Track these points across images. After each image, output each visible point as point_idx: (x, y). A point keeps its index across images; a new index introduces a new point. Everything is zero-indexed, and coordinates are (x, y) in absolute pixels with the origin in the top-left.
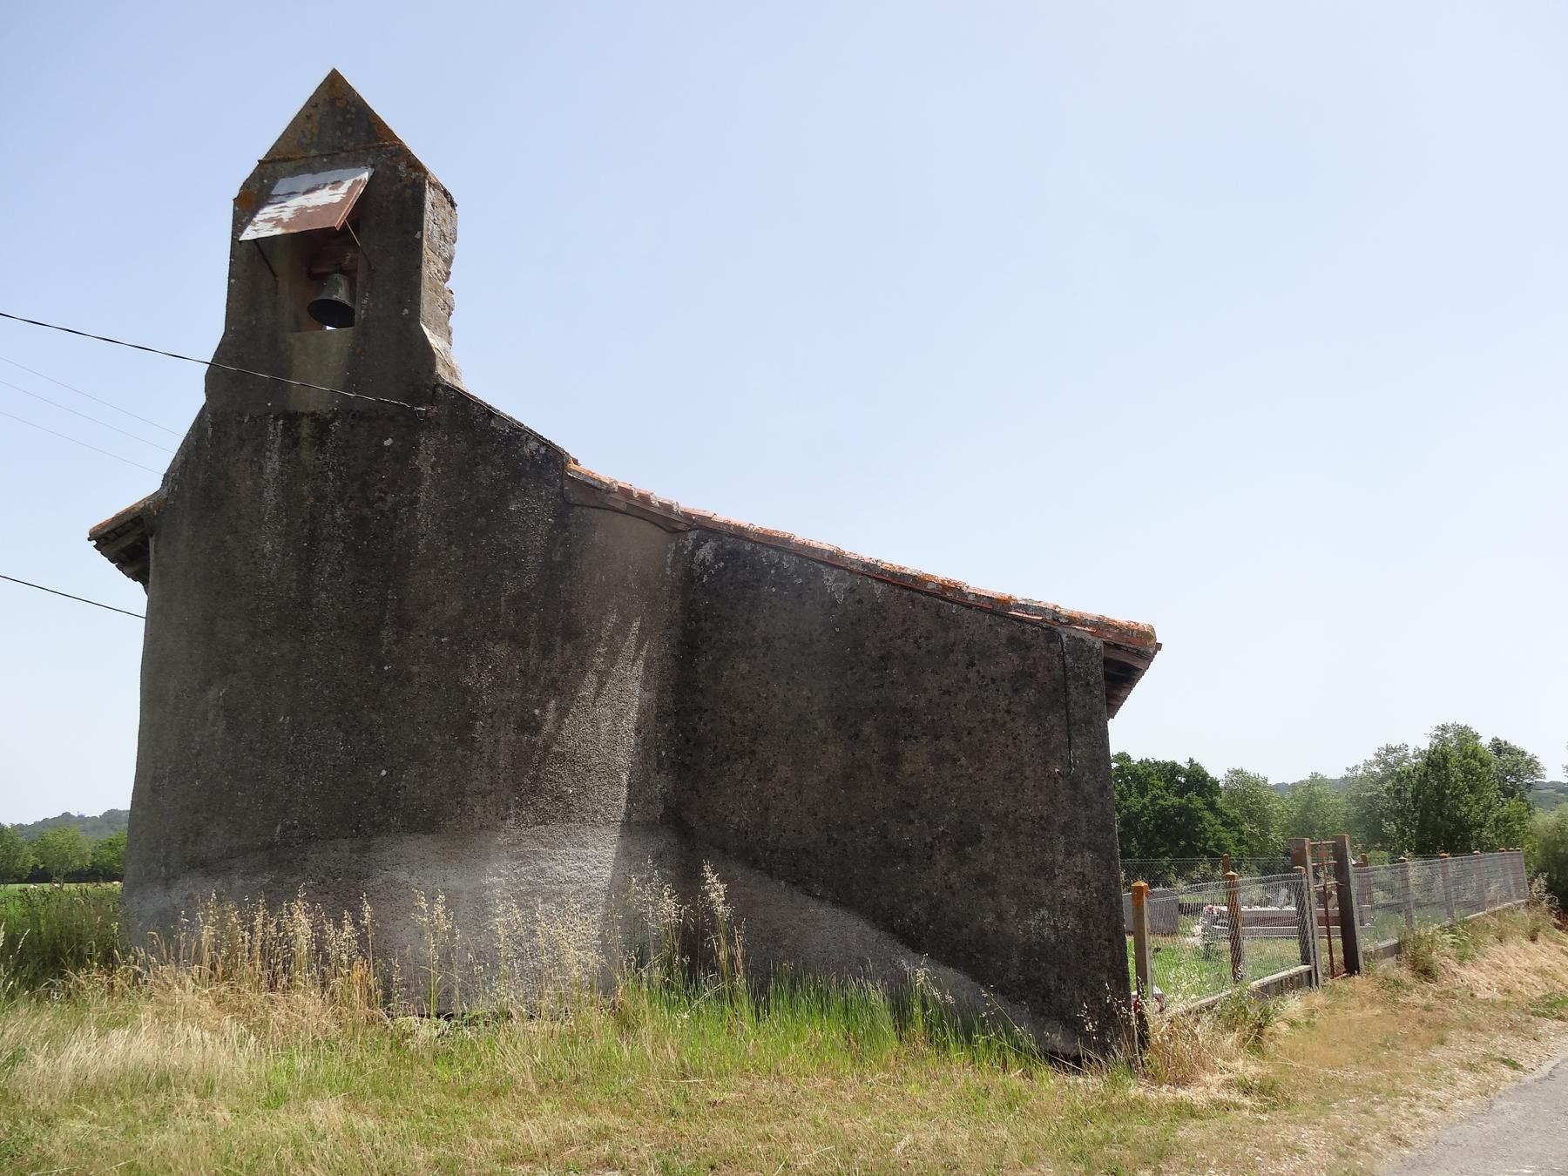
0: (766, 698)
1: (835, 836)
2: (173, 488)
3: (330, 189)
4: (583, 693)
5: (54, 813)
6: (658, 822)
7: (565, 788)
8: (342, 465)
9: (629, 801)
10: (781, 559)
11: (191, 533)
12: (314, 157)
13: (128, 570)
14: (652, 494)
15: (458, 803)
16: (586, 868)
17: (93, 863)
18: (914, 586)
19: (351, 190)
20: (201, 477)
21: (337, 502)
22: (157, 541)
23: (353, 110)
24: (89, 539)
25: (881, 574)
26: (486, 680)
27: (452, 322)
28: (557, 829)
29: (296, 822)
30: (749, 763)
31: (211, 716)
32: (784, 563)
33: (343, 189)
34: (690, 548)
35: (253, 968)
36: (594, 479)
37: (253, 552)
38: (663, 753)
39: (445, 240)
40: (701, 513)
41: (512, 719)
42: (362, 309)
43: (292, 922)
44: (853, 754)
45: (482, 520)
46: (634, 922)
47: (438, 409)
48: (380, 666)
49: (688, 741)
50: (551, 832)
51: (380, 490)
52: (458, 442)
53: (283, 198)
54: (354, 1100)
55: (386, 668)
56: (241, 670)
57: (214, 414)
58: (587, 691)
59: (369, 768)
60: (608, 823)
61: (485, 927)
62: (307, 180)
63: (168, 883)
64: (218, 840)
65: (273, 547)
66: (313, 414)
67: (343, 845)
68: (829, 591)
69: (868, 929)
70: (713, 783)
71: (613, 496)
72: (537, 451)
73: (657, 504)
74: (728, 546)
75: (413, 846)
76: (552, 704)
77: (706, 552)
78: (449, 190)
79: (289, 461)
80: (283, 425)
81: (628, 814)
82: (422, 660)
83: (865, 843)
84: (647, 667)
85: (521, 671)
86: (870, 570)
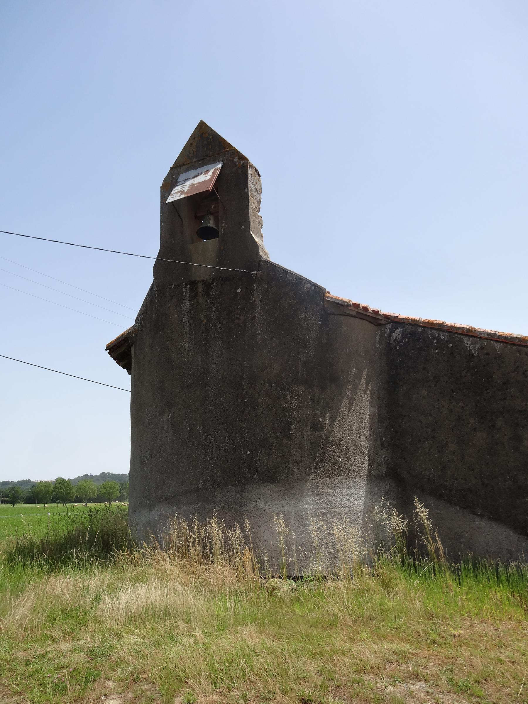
0: (438, 408)
1: (486, 481)
2: (141, 323)
3: (204, 174)
4: (342, 409)
5: (82, 474)
6: (384, 475)
7: (338, 458)
8: (219, 304)
9: (369, 464)
10: (439, 335)
11: (150, 342)
12: (195, 162)
13: (121, 364)
14: (368, 306)
15: (286, 467)
16: (351, 500)
17: (97, 495)
18: (519, 343)
19: (214, 173)
21: (217, 321)
22: (135, 348)
23: (211, 137)
24: (106, 350)
25: (498, 338)
26: (295, 404)
27: (263, 231)
29: (208, 478)
30: (432, 443)
31: (165, 428)
32: (441, 336)
33: (210, 173)
34: (388, 333)
35: (195, 550)
36: (340, 300)
37: (180, 349)
38: (384, 439)
39: (257, 192)
40: (392, 315)
41: (309, 424)
43: (211, 528)
44: (492, 437)
45: (286, 325)
46: (379, 529)
47: (262, 272)
48: (243, 400)
49: (396, 432)
50: (333, 481)
51: (237, 314)
52: (272, 287)
53: (183, 182)
54: (261, 626)
55: (246, 400)
56: (178, 405)
57: (158, 286)
58: (344, 408)
59: (241, 451)
60: (360, 476)
61: (304, 531)
62: (193, 172)
63: (150, 508)
64: (172, 487)
65: (189, 345)
66: (203, 281)
67: (232, 489)
68: (468, 349)
69: (512, 533)
70: (413, 454)
71: (350, 308)
73: (371, 311)
74: (409, 330)
75: (266, 489)
76: (328, 416)
77: (397, 334)
78: (257, 168)
79: (193, 304)
81: (369, 471)
82: (263, 396)
83: (505, 485)
84: (372, 395)
86: (492, 336)
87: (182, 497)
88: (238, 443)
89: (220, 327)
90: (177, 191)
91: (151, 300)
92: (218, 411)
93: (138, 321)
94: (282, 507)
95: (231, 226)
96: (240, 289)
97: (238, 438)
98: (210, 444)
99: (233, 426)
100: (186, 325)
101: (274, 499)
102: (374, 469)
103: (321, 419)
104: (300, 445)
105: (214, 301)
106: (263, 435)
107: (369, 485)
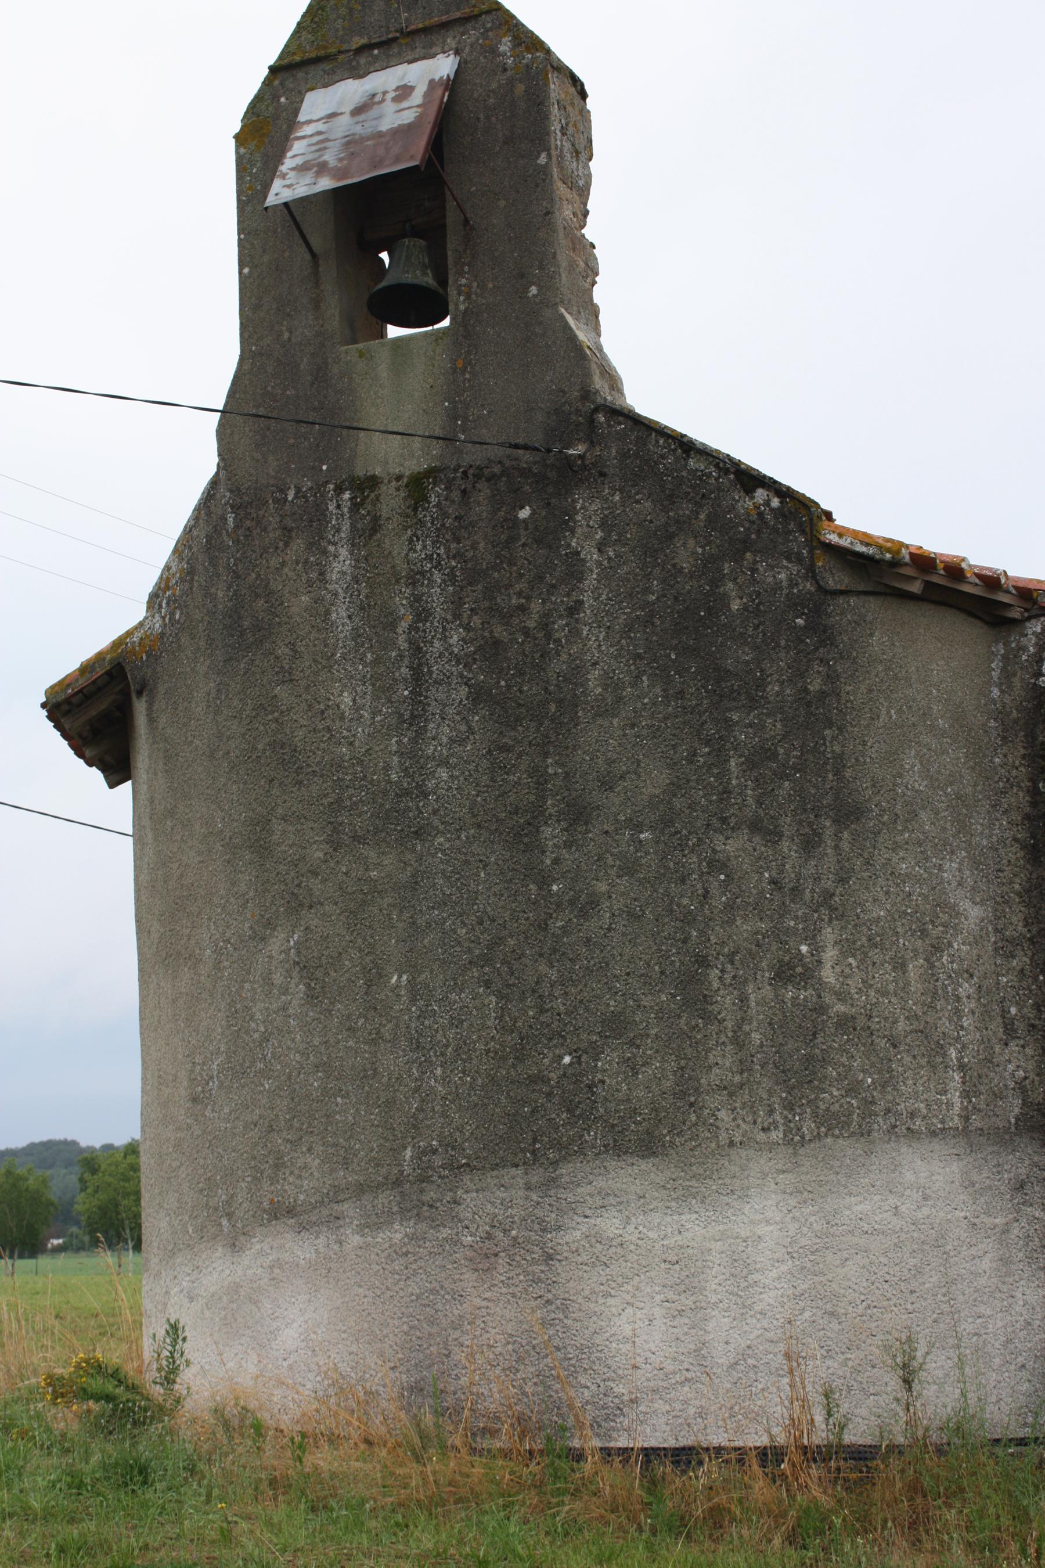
6: (1013, 1129)
8: (454, 557)
15: (691, 1105)
20: (220, 594)
28: (846, 1148)
29: (434, 1143)
31: (278, 978)
37: (322, 712)
38: (1013, 1010)
42: (459, 294)
48: (544, 883)
52: (638, 502)
57: (236, 491)
65: (354, 700)
72: (767, 503)
80: (351, 499)
82: (613, 872)
85: (773, 881)
87: (346, 1206)
88: (531, 1026)
89: (463, 640)
90: (299, 161)
91: (209, 538)
92: (462, 922)
93: (160, 606)
94: (680, 1232)
95: (490, 286)
96: (527, 508)
97: (531, 1013)
98: (437, 1031)
99: (512, 973)
100: (342, 631)
101: (651, 1207)
102: (979, 1110)
103: (804, 949)
104: (734, 1032)
105: (438, 548)
106: (612, 1003)
107: (962, 1159)
